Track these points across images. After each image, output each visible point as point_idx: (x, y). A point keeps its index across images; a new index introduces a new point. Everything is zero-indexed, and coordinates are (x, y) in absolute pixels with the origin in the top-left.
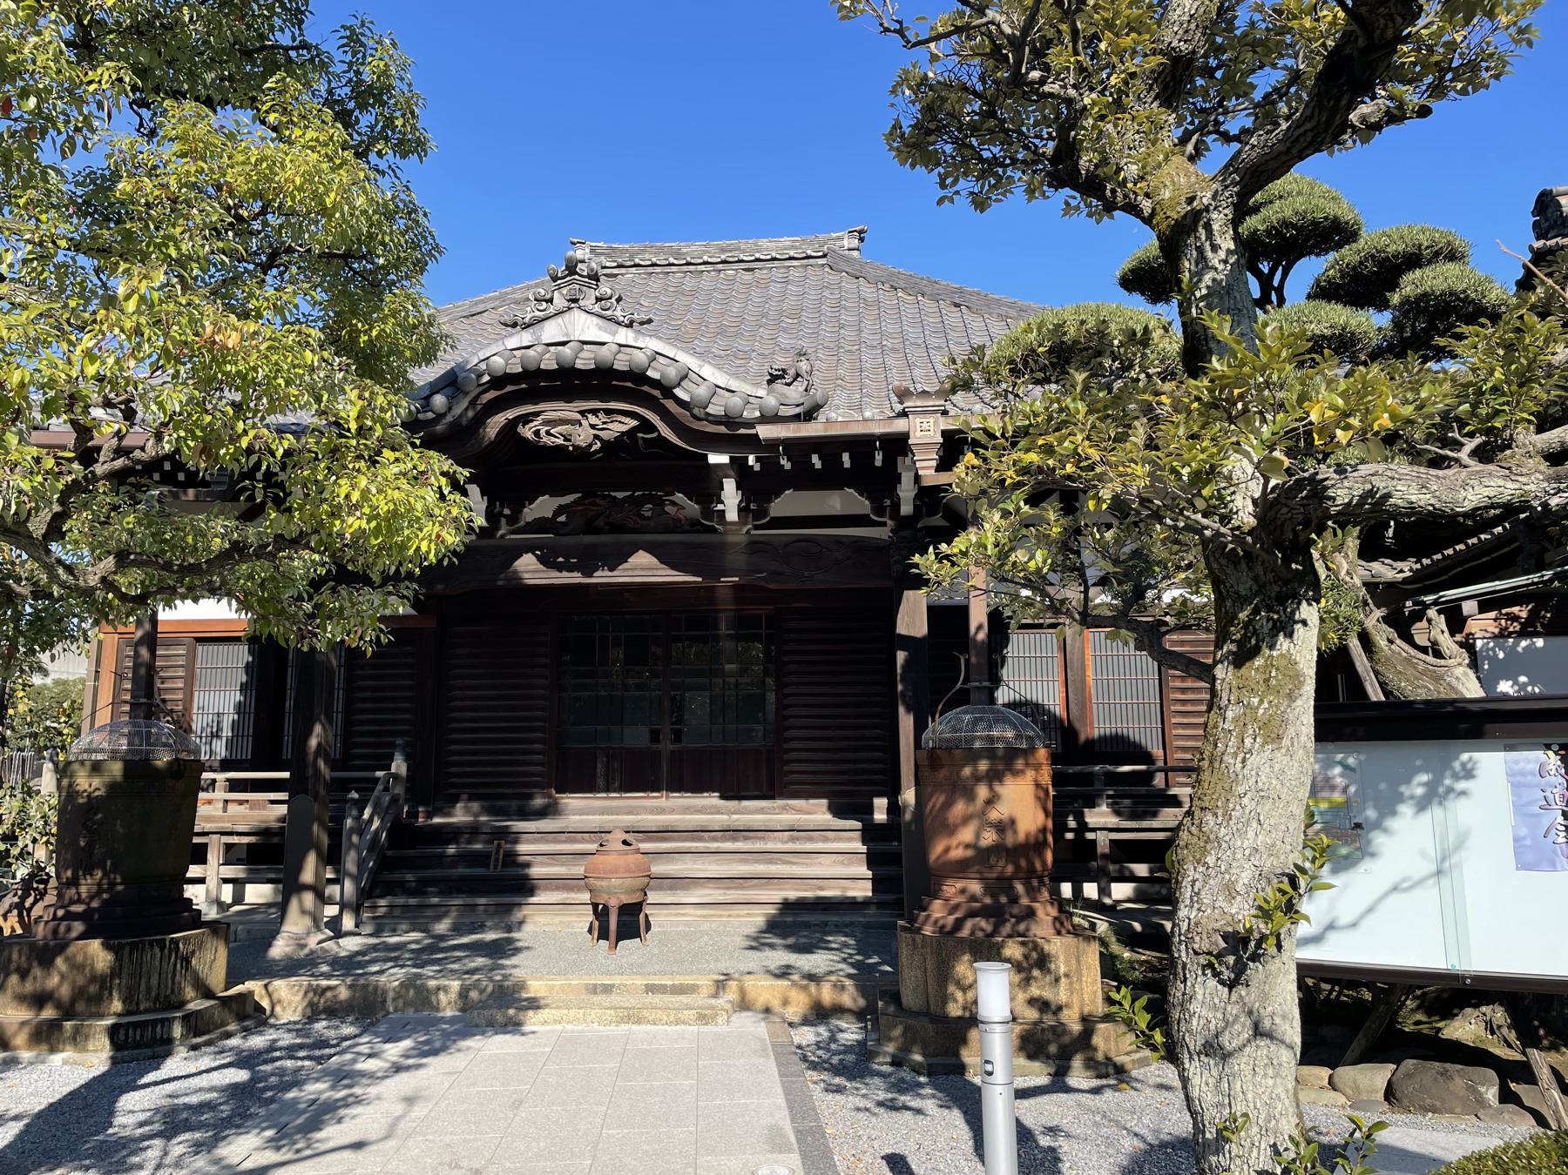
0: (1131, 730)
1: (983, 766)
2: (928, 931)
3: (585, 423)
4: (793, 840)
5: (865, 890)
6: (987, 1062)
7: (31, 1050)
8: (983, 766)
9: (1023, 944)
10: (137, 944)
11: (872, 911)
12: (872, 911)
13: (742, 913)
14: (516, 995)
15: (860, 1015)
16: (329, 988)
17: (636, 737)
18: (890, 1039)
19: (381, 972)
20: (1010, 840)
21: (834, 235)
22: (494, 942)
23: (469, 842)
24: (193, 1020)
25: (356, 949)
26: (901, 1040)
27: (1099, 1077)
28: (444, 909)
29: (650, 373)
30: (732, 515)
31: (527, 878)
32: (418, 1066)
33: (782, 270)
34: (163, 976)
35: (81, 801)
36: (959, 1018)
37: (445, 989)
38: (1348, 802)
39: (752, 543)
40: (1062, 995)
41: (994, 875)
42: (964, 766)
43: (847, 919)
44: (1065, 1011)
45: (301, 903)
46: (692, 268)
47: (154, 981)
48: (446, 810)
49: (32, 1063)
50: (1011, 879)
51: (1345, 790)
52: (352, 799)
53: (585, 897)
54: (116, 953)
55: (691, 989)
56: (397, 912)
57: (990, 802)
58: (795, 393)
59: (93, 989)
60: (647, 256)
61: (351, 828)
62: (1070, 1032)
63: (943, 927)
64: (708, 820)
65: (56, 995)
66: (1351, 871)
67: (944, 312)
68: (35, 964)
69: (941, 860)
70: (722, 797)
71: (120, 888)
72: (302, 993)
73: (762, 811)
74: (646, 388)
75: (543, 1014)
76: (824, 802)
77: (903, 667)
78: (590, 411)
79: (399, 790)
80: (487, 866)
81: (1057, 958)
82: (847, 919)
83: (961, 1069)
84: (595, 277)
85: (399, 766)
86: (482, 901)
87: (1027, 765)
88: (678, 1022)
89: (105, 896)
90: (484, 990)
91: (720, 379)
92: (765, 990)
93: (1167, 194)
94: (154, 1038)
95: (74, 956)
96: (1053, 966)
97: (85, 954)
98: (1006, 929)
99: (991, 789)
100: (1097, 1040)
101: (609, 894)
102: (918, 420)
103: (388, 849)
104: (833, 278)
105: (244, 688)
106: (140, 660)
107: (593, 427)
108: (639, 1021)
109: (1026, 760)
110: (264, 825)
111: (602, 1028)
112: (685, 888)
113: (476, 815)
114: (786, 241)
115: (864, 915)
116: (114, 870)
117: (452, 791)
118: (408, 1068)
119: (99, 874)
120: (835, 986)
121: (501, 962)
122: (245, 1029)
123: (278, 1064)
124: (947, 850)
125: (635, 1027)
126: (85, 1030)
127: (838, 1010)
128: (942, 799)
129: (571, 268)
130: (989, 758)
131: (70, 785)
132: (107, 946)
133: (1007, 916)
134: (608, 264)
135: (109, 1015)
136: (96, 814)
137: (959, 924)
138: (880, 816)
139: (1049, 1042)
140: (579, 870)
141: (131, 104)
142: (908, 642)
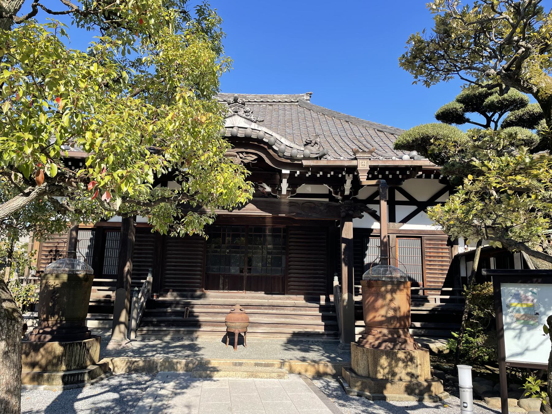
0: (411, 274)
1: (389, 287)
2: (367, 346)
3: (238, 156)
4: (294, 310)
5: (321, 329)
6: (464, 403)
7: (31, 384)
8: (389, 287)
9: (405, 352)
10: (72, 344)
11: (325, 337)
12: (325, 337)
13: (278, 336)
14: (207, 366)
15: (334, 376)
16: (136, 361)
17: (234, 270)
18: (355, 386)
19: (153, 356)
20: (398, 315)
21: (301, 95)
22: (189, 345)
23: (175, 307)
24: (91, 373)
25: (139, 346)
26: (360, 387)
27: (434, 402)
28: (168, 332)
29: (264, 140)
30: (284, 192)
31: (198, 321)
32: (183, 393)
33: (282, 106)
34: (81, 356)
35: (51, 289)
36: (382, 379)
37: (180, 363)
38: (533, 305)
39: (290, 202)
40: (418, 372)
41: (392, 327)
42: (382, 287)
43: (316, 340)
44: (420, 378)
45: (119, 328)
46: (250, 103)
47: (77, 358)
48: (164, 295)
49: (31, 390)
50: (398, 328)
51: (532, 301)
52: (136, 290)
53: (224, 329)
54: (64, 347)
55: (272, 365)
56: (150, 333)
57: (391, 300)
58: (315, 149)
59: (55, 361)
60: (266, 99)
61: (135, 301)
62: (423, 385)
63: (373, 345)
64: (251, 301)
65: (40, 363)
66: (535, 329)
67: (343, 124)
68: (32, 351)
69: (372, 321)
70: (266, 293)
71: (64, 322)
72: (125, 363)
73: (280, 299)
74: (262, 145)
75: (220, 373)
76: (303, 296)
77: (344, 249)
78: (240, 152)
79: (150, 287)
80: (183, 316)
81: (417, 358)
82: (316, 340)
83: (384, 398)
84: (243, 104)
85: (150, 278)
86: (182, 329)
87: (404, 287)
88: (270, 377)
89: (58, 325)
90: (195, 364)
91: (288, 143)
92: (299, 366)
93: (544, 85)
94: (78, 380)
95: (48, 348)
96: (415, 361)
97: (52, 347)
98: (398, 347)
99: (392, 296)
100: (433, 388)
101: (235, 328)
102: (361, 161)
103: (146, 309)
104: (301, 109)
105: (89, 247)
106: (73, 236)
107: (241, 158)
108: (256, 377)
109: (404, 286)
110: (98, 299)
111: (242, 379)
112: (257, 327)
113: (175, 297)
114: (284, 96)
115: (322, 338)
116: (62, 315)
117: (166, 288)
118: (179, 394)
119: (57, 317)
120: (324, 365)
121: (196, 353)
122: (107, 377)
123: (127, 391)
124: (375, 317)
125: (255, 379)
126: (52, 377)
127: (326, 374)
128: (373, 298)
129: (236, 100)
130: (391, 284)
131: (46, 283)
132: (61, 345)
133: (398, 342)
134: (220, 100)
135: (60, 371)
136: (56, 294)
137: (380, 345)
138: (323, 302)
139: (415, 389)
140: (223, 319)
141: (101, 29)
142: (346, 240)
